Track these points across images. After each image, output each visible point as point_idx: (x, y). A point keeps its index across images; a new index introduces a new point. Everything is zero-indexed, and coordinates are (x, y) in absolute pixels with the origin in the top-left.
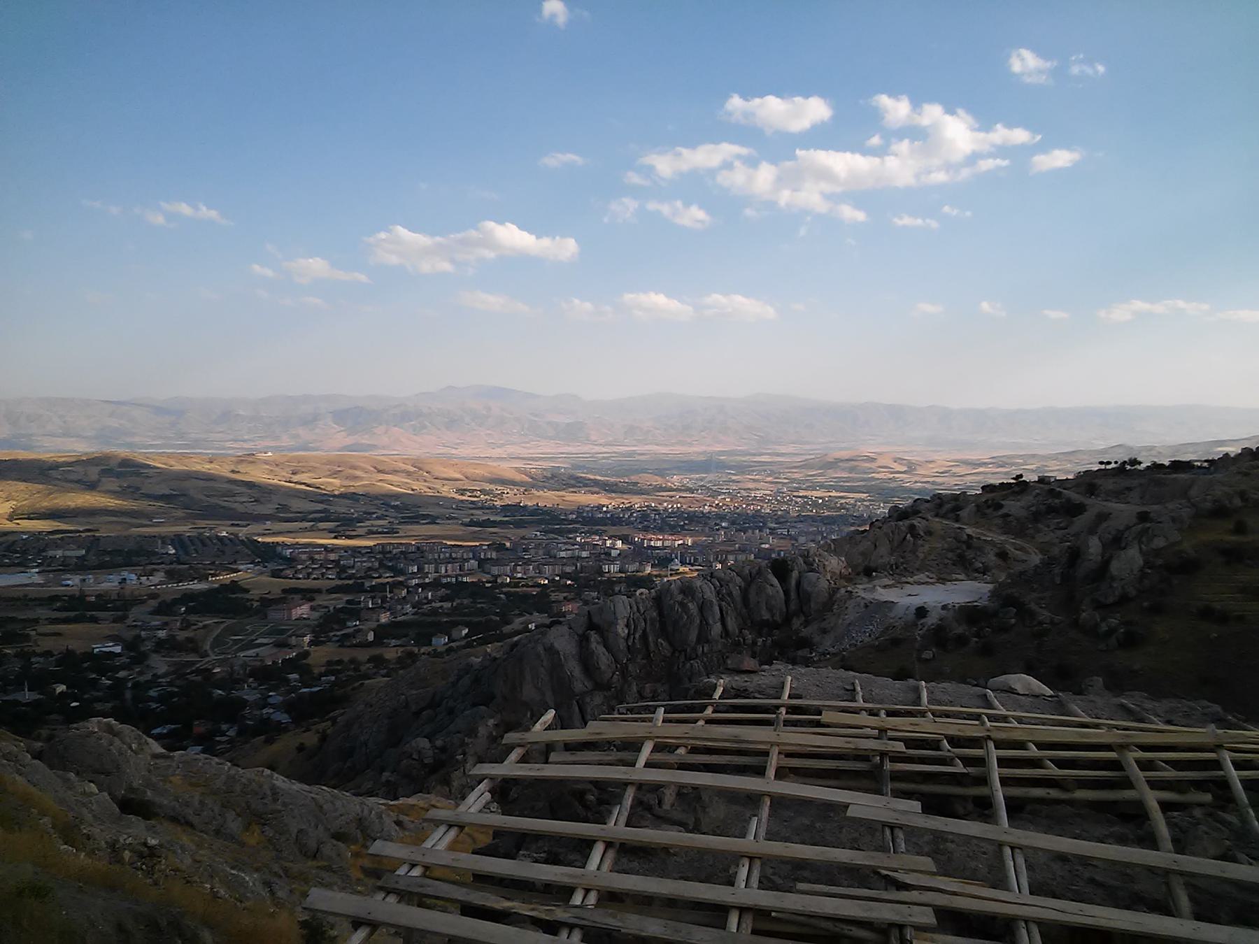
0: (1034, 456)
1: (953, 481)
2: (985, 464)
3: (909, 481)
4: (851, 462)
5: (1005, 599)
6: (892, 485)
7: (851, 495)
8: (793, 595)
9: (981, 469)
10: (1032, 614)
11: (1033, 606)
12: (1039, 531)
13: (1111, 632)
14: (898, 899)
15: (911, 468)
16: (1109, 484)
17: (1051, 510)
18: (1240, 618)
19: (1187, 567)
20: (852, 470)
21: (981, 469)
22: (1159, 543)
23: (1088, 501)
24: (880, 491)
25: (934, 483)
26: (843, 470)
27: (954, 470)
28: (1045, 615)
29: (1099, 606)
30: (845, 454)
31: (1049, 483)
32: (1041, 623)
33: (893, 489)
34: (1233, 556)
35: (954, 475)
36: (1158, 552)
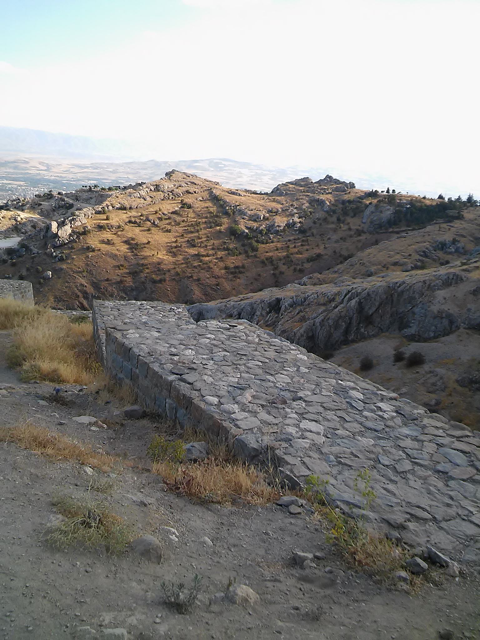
0: (112, 164)
1: (71, 176)
2: (87, 167)
3: (48, 175)
4: (14, 164)
5: (22, 245)
6: (38, 177)
7: (15, 183)
8: (402, 437)
9: (85, 170)
10: (31, 250)
11: (32, 247)
12: (54, 215)
13: (56, 257)
14: (451, 434)
15: (48, 168)
16: (85, 196)
17: (59, 207)
18: (99, 250)
19: (85, 233)
20: (16, 168)
21: (85, 170)
22: (78, 224)
23: (75, 203)
24: (34, 182)
25: (61, 177)
26: (10, 168)
27: (72, 170)
28: (35, 250)
29: (55, 247)
30: (11, 158)
31: (62, 195)
32: (34, 254)
33: (39, 180)
35: (72, 173)
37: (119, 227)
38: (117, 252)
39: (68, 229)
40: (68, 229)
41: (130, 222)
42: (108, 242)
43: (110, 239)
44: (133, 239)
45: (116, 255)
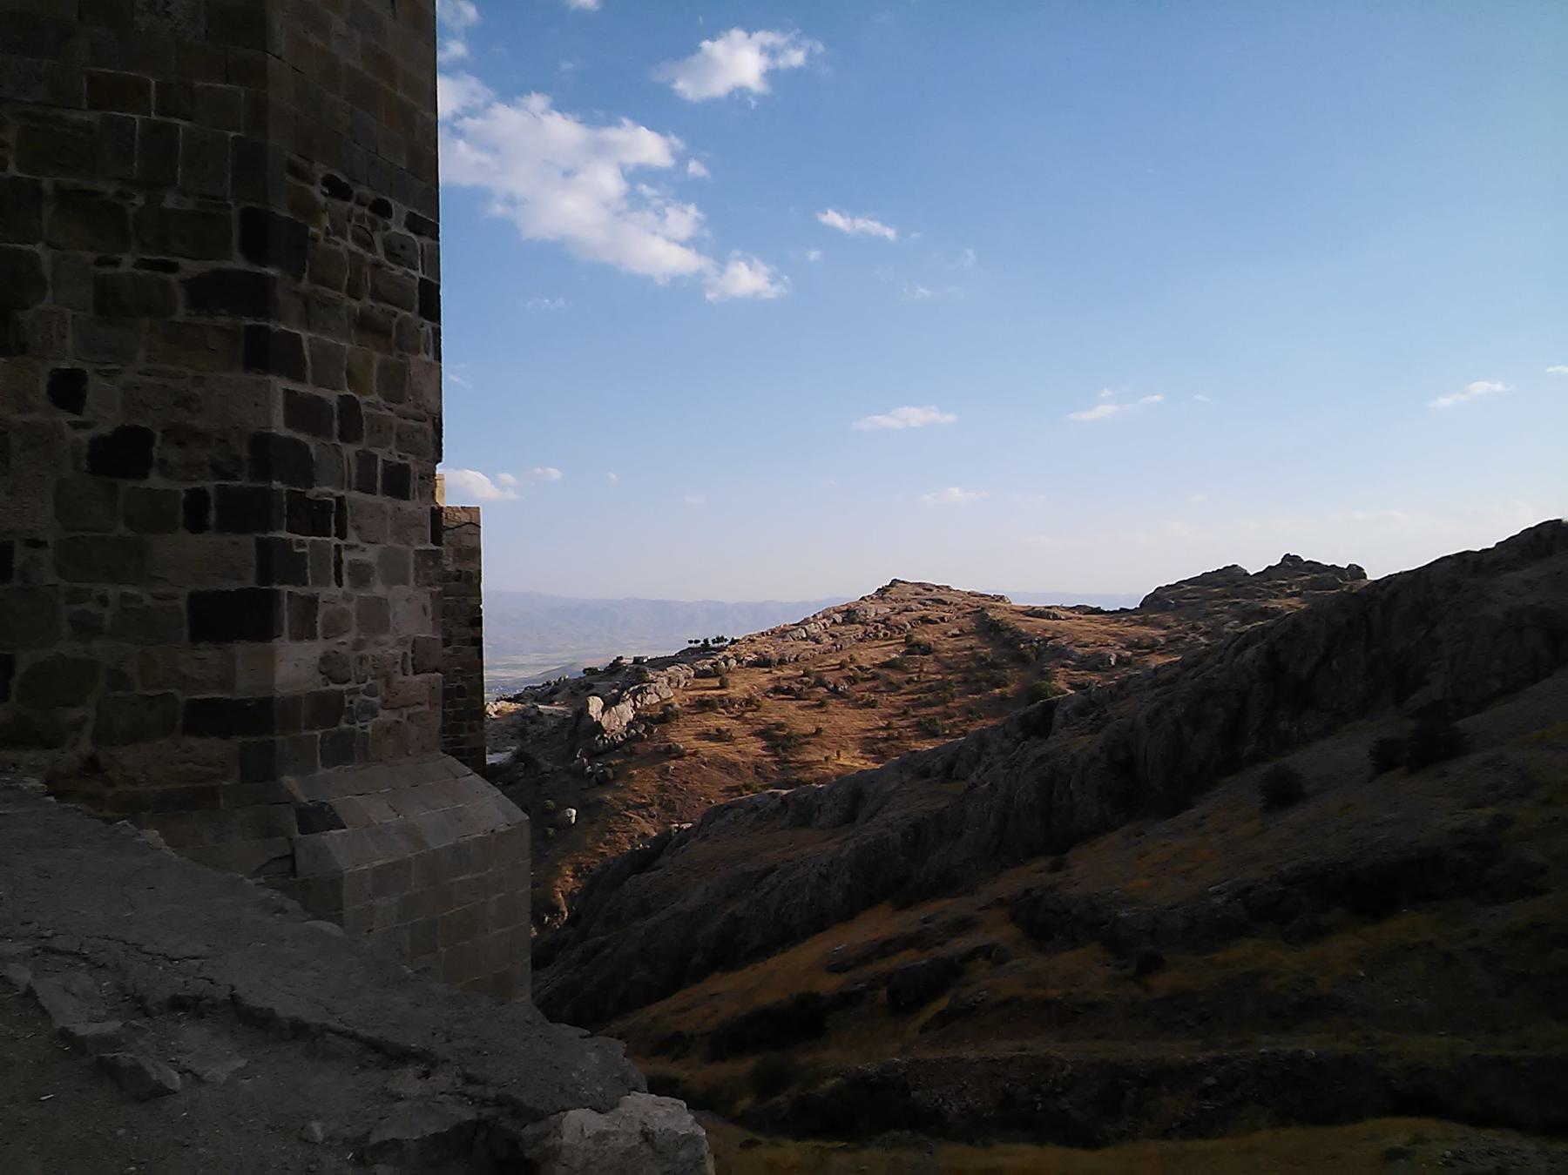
22: (652, 699)
28: (548, 766)
34: (703, 705)
36: (648, 708)
37: (749, 702)
38: (738, 757)
39: (626, 711)
40: (626, 711)
41: (777, 690)
42: (720, 736)
43: (724, 728)
44: (780, 726)
45: (735, 764)
